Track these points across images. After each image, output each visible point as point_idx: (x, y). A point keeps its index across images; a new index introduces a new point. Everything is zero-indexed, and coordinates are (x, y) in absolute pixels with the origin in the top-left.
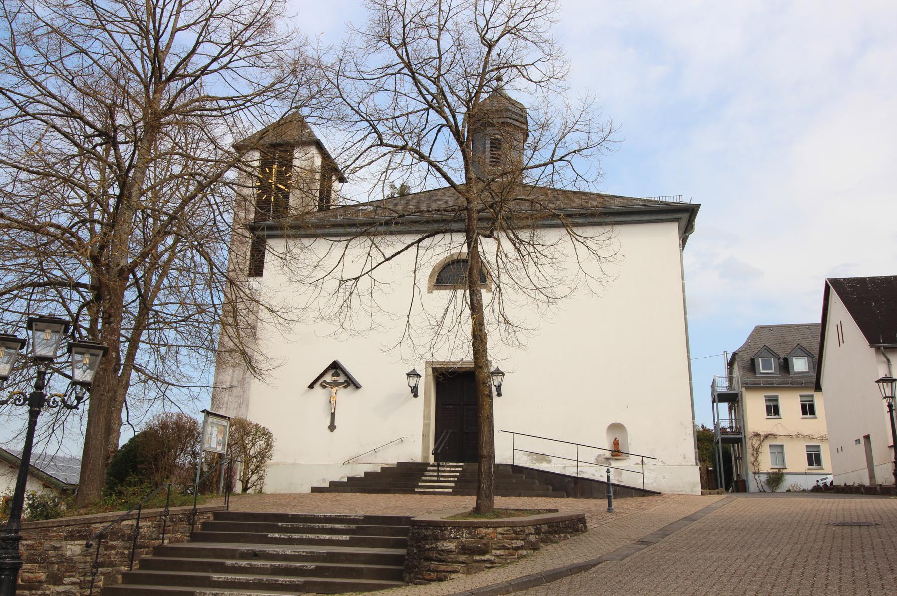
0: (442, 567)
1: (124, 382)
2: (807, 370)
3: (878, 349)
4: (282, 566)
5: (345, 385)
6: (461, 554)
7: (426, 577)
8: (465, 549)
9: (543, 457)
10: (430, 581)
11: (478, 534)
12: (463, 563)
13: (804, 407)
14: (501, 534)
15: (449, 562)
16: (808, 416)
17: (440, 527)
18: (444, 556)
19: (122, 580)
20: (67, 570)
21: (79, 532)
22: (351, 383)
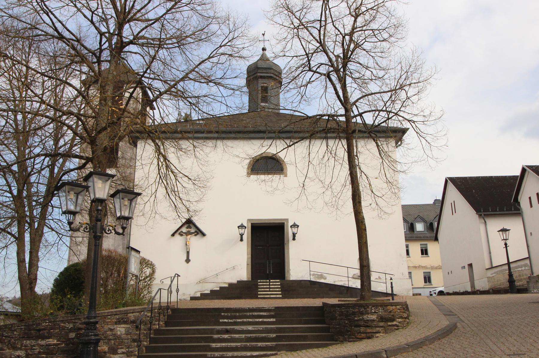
0: (369, 330)
1: (40, 232)
2: (423, 230)
3: (480, 216)
4: (253, 336)
5: (196, 234)
6: (380, 322)
7: (358, 337)
8: (382, 319)
9: (321, 276)
10: (361, 339)
11: (389, 310)
12: (382, 327)
13: (422, 251)
14: (399, 309)
15: (373, 327)
16: (424, 256)
17: (364, 306)
18: (369, 324)
19: (146, 351)
20: (119, 345)
21: (122, 319)
22: (199, 232)
